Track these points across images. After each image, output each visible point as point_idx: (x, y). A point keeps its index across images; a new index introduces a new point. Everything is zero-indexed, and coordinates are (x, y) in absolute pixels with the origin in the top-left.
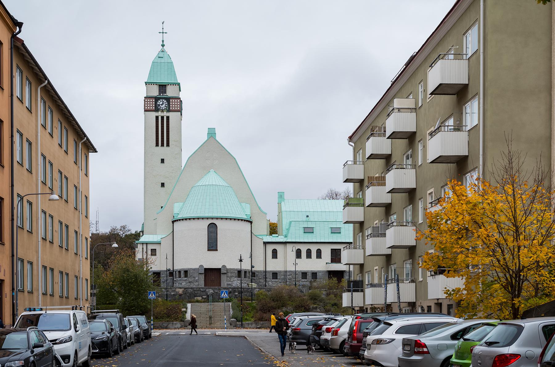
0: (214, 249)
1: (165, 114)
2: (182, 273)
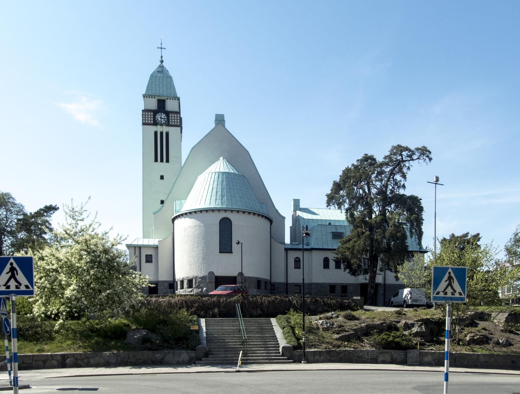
1: (165, 129)
2: (185, 283)
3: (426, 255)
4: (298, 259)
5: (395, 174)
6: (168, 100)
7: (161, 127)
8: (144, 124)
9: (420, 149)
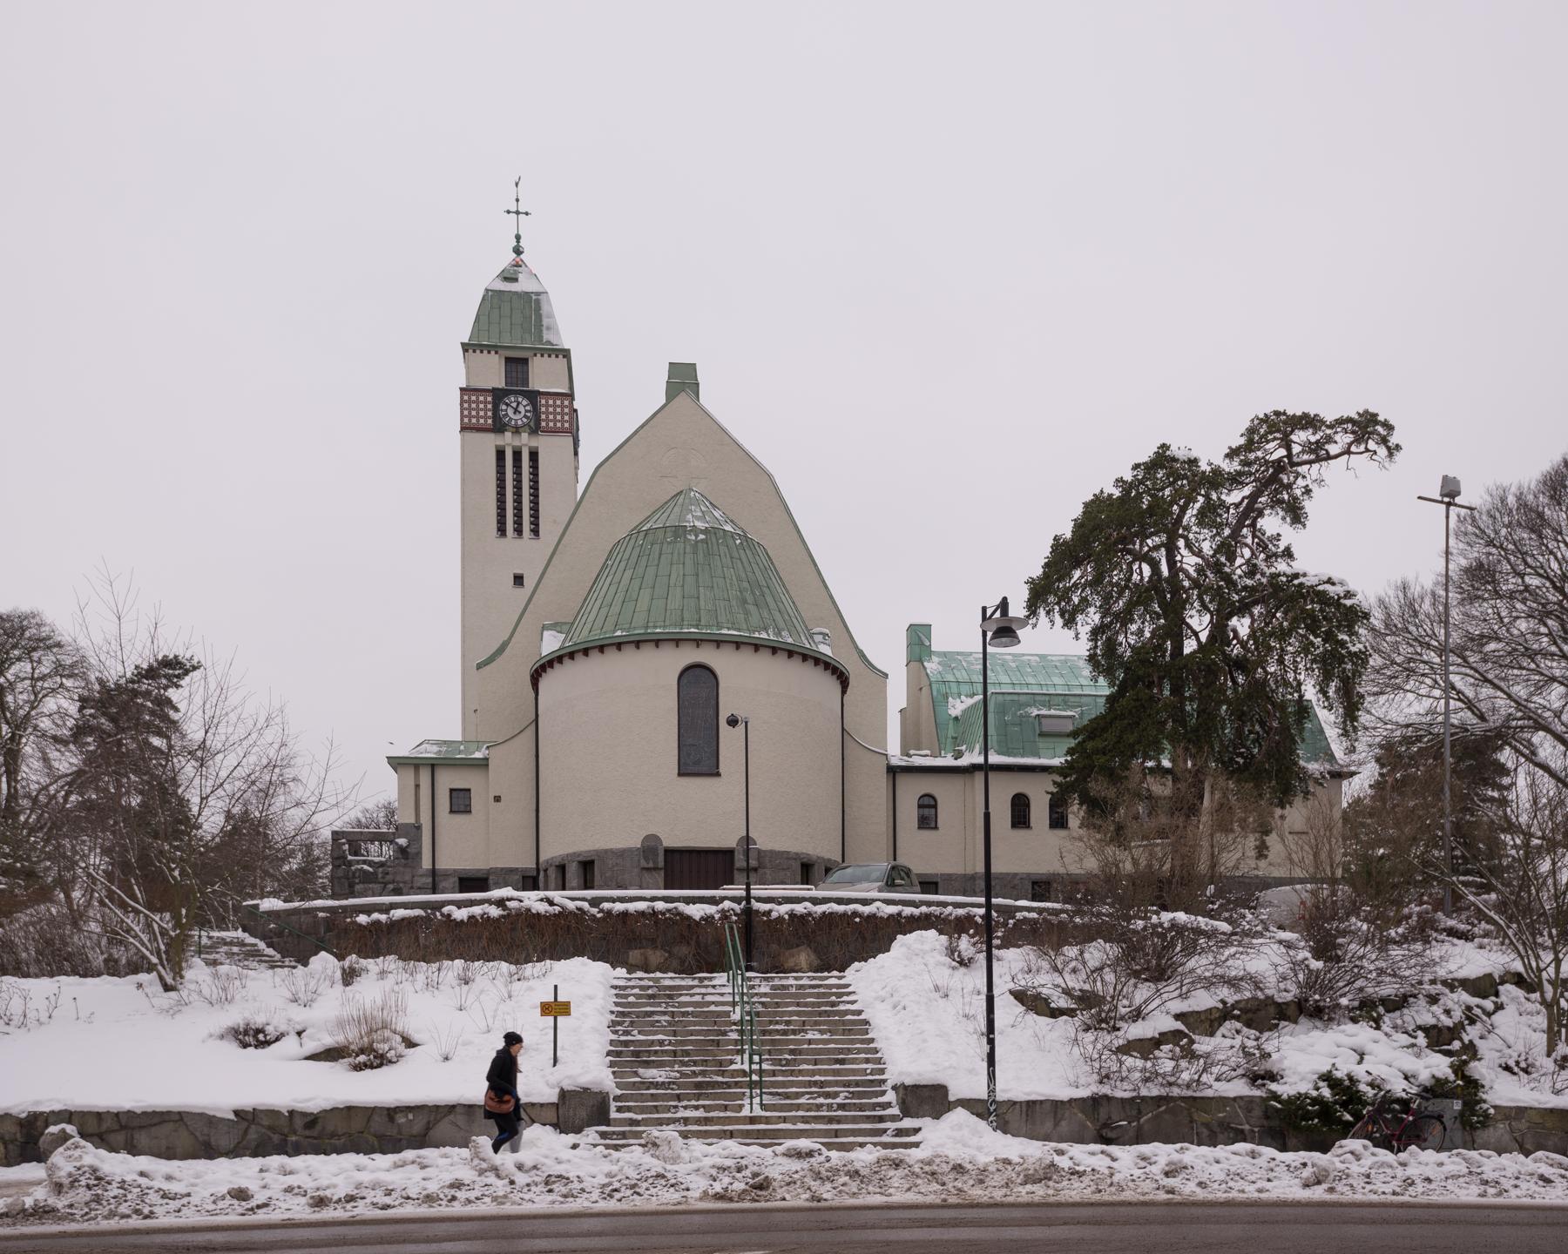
0: (705, 769)
3: (1345, 783)
4: (927, 801)
5: (1261, 514)
8: (464, 429)
9: (1350, 420)
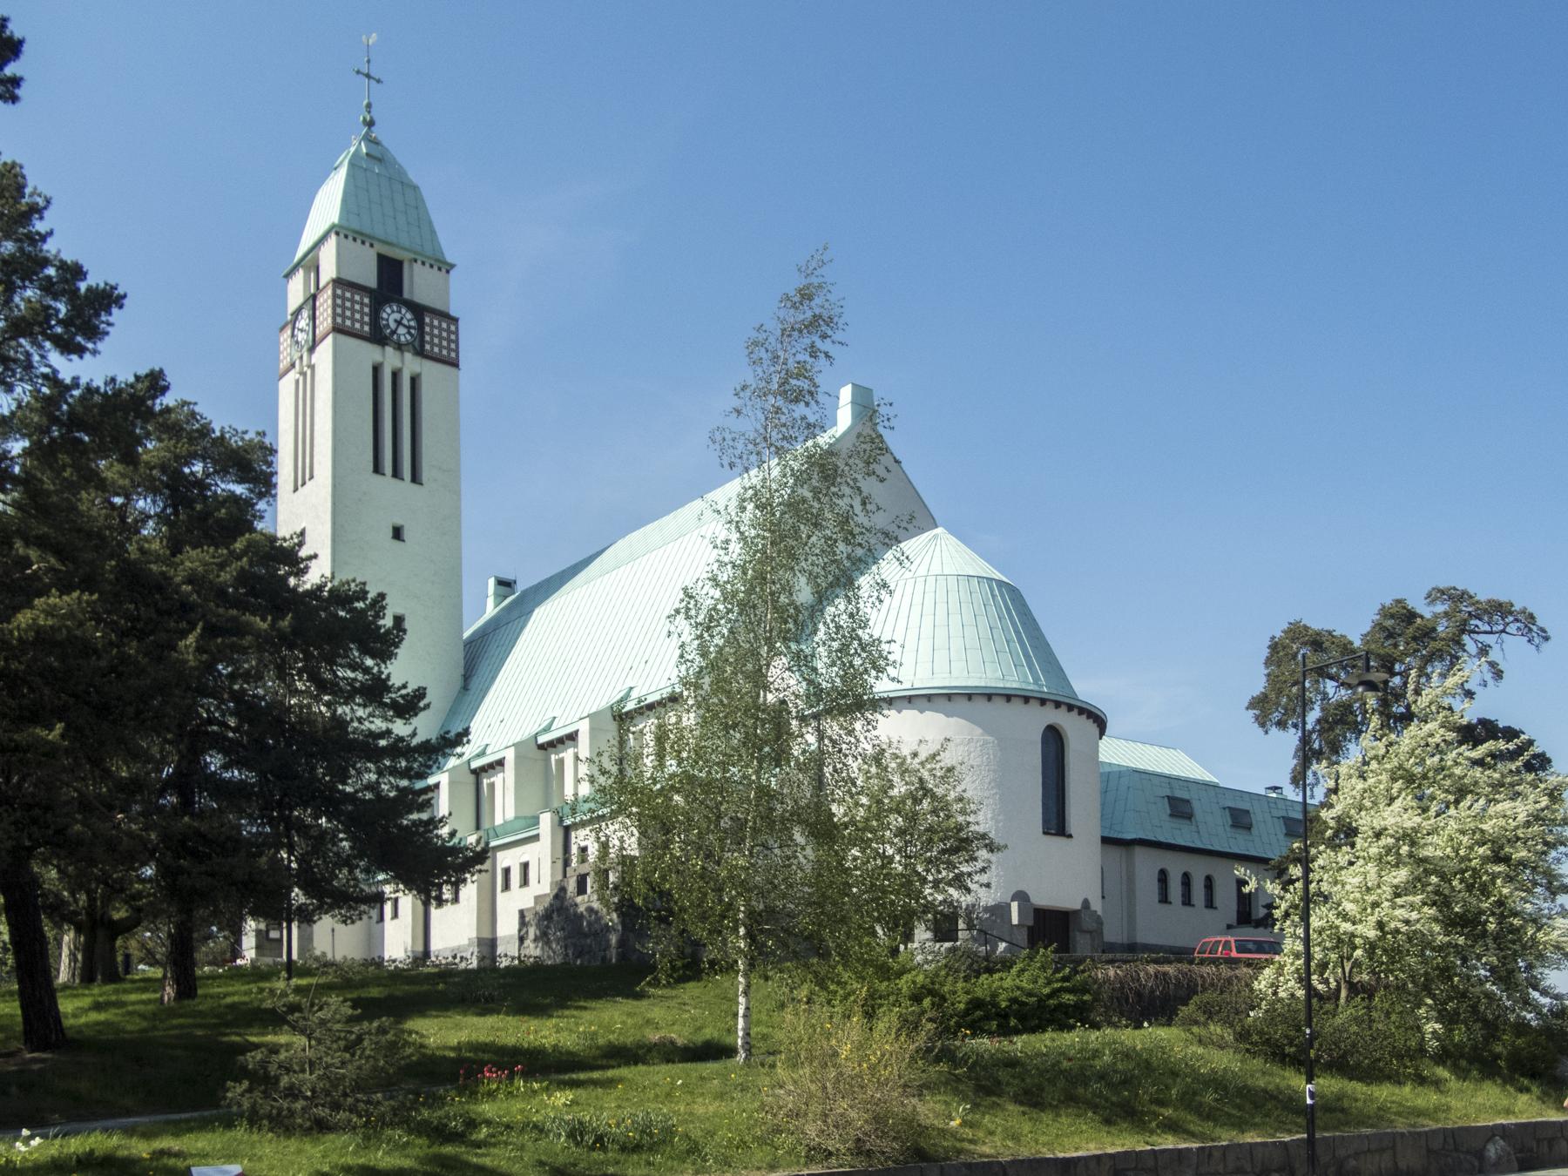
6: (417, 267)
7: (398, 353)
